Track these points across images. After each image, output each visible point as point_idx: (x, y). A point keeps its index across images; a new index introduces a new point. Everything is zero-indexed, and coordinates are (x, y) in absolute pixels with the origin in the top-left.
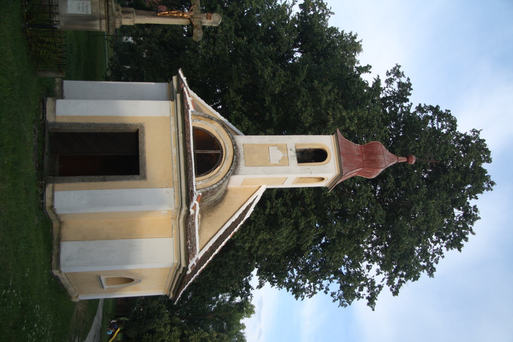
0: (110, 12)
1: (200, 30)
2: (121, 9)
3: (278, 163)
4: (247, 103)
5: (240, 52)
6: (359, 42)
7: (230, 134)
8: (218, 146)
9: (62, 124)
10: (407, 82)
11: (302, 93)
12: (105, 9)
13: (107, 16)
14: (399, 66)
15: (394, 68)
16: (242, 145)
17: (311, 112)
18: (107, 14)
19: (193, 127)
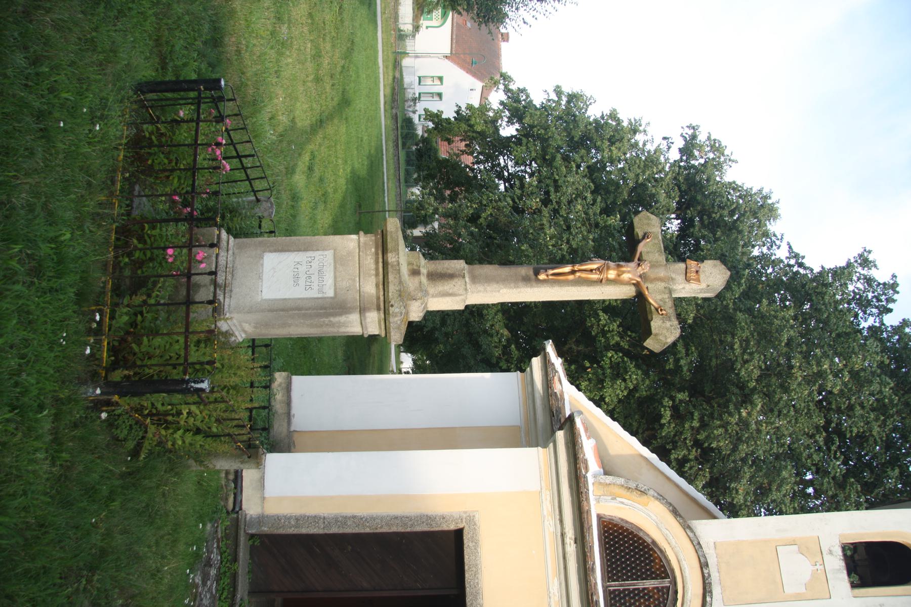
0: (392, 289)
1: (670, 320)
2: (425, 266)
3: (803, 590)
4: (629, 334)
5: (613, 241)
6: (773, 204)
7: (691, 535)
8: (663, 566)
9: (278, 518)
10: (892, 282)
11: (740, 323)
12: (377, 275)
13: (382, 298)
14: (870, 252)
15: (859, 255)
16: (712, 544)
17: (759, 361)
18: (382, 293)
19: (599, 517)
